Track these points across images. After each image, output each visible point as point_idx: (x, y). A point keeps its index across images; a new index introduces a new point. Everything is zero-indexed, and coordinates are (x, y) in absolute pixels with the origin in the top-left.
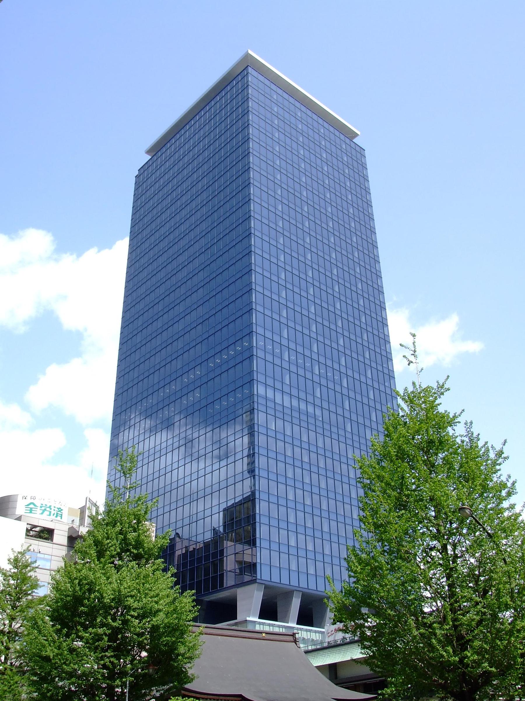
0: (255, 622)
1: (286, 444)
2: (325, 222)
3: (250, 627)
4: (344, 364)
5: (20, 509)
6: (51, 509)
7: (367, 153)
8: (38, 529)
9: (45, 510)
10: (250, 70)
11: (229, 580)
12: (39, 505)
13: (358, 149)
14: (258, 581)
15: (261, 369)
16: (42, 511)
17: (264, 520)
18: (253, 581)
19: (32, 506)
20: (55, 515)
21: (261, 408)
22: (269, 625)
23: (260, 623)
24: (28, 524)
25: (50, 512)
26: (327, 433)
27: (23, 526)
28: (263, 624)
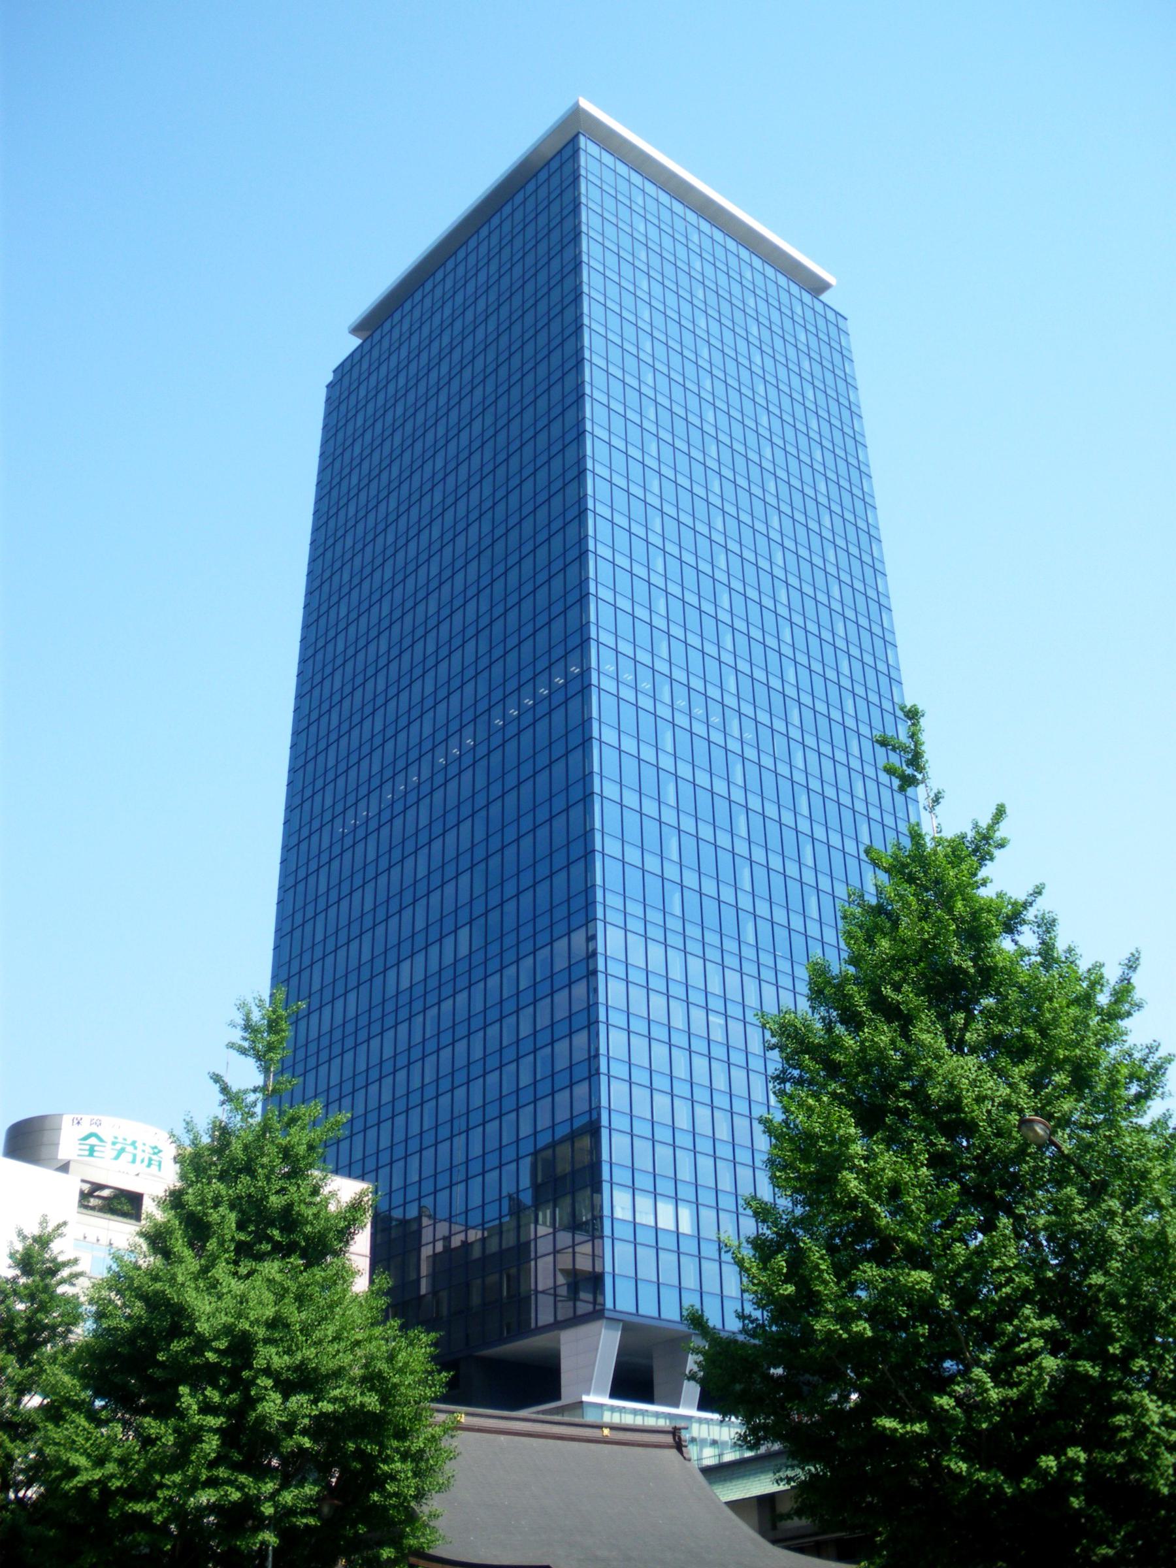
0: (601, 1406)
1: (676, 1100)
2: (755, 447)
3: (590, 1417)
4: (810, 863)
5: (68, 1145)
6: (136, 1148)
7: (851, 326)
8: (106, 1193)
9: (123, 1150)
10: (582, 139)
11: (545, 1317)
12: (108, 1138)
13: (831, 316)
14: (607, 1314)
15: (613, 826)
16: (115, 1153)
17: (617, 1019)
18: (597, 1313)
19: (93, 1141)
20: (146, 1163)
21: (613, 917)
22: (635, 1412)
23: (613, 1409)
24: (83, 1181)
25: (135, 1156)
26: (768, 975)
27: (72, 1185)
28: (621, 1410)
